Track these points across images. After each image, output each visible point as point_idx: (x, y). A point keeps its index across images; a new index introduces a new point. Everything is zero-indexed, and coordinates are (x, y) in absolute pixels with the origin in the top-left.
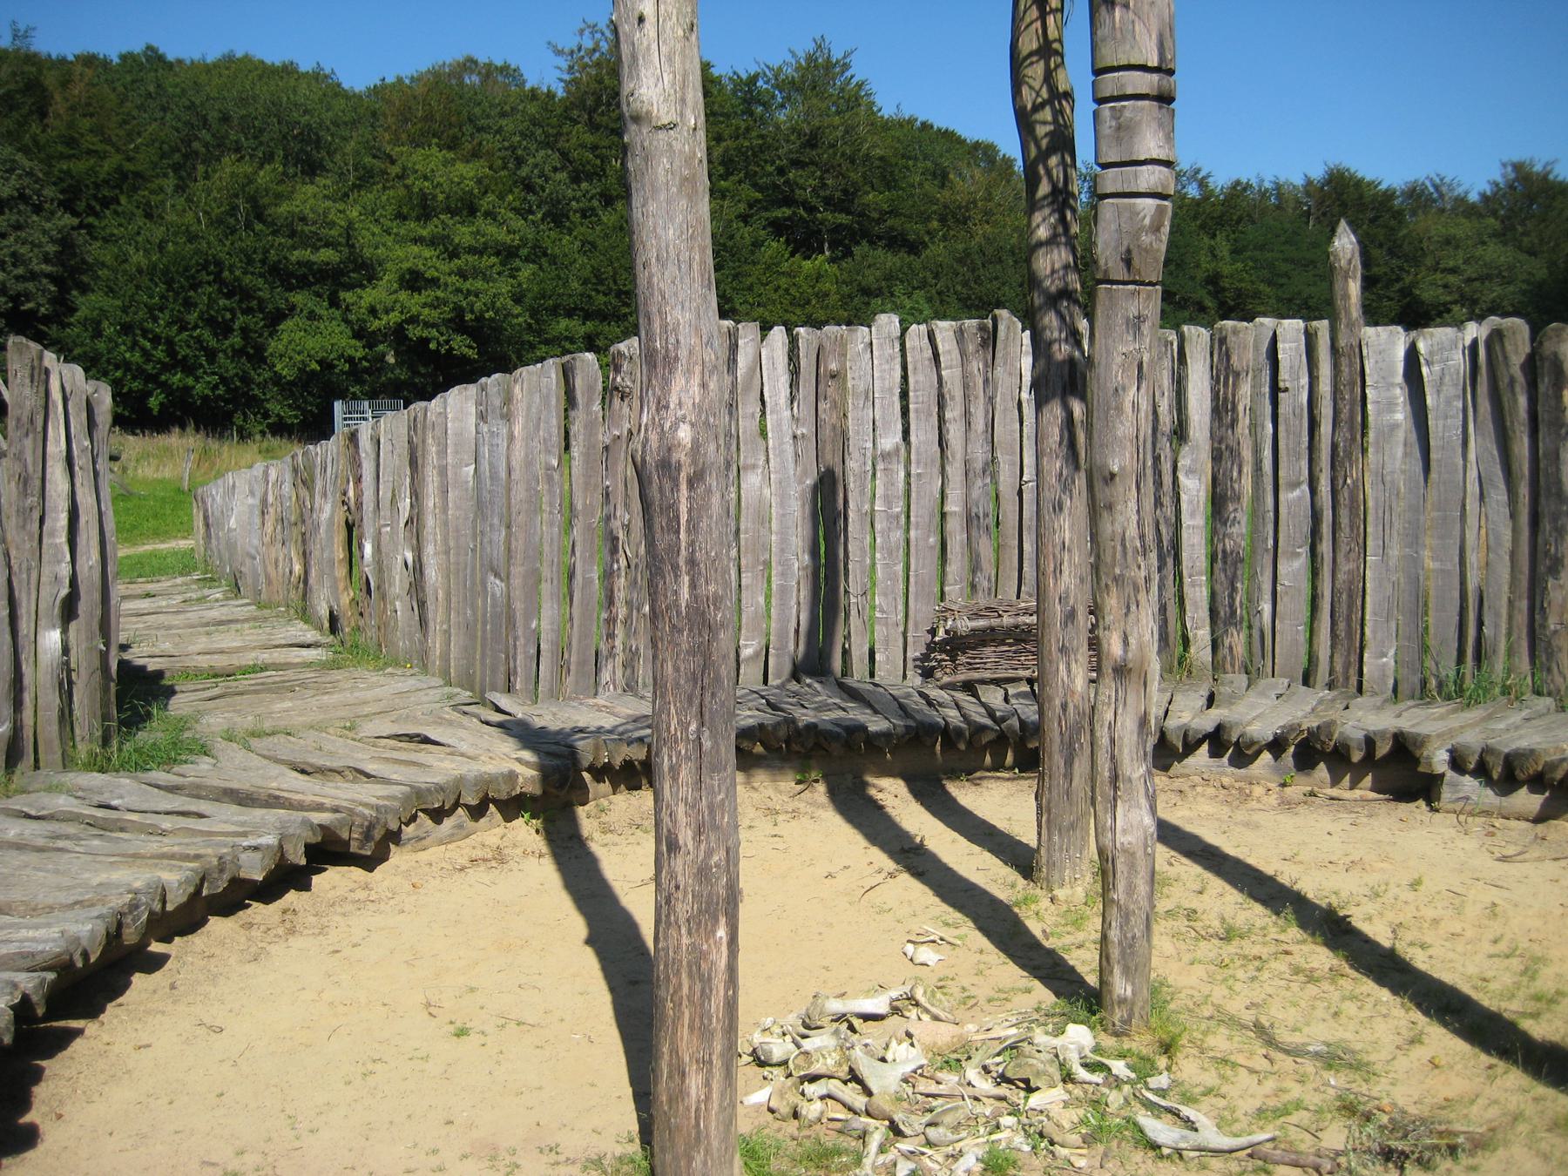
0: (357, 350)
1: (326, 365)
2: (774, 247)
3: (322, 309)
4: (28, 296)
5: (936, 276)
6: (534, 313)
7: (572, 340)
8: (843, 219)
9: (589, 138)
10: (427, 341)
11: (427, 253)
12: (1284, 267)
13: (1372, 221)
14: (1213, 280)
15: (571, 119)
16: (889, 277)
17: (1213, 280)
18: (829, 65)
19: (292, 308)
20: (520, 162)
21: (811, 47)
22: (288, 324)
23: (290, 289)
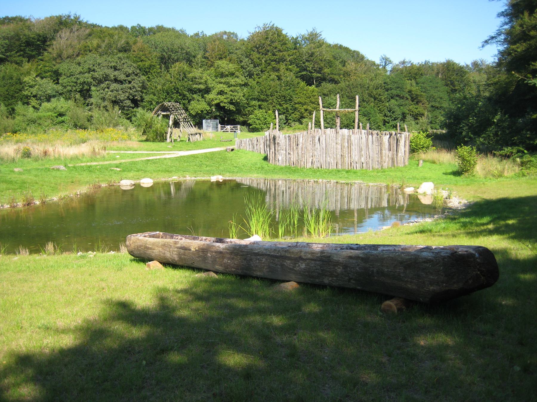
0: (208, 108)
1: (202, 111)
2: (303, 84)
3: (200, 98)
4: (136, 96)
5: (341, 90)
6: (247, 99)
7: (256, 106)
8: (319, 75)
9: (258, 56)
10: (225, 106)
11: (224, 86)
14: (410, 92)
15: (253, 50)
18: (316, 34)
19: (194, 98)
20: (241, 61)
21: (311, 30)
22: (192, 102)
23: (193, 94)
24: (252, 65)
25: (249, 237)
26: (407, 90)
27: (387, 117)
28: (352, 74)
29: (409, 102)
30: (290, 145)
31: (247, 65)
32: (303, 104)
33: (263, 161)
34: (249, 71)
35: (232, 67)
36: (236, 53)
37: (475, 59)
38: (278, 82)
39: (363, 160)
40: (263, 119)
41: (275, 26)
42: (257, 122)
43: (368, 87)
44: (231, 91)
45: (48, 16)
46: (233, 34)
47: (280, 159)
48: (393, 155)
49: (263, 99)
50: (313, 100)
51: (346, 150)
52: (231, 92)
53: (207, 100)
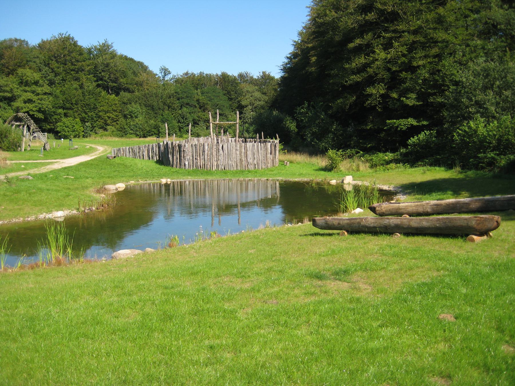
12: (213, 97)
16: (129, 100)
17: (198, 100)
18: (108, 46)
24: (53, 75)
25: (335, 212)
26: (195, 99)
27: (181, 123)
28: (145, 84)
29: (197, 109)
30: (196, 152)
31: (47, 74)
32: (106, 112)
33: (158, 166)
34: (50, 80)
35: (37, 76)
36: (35, 62)
37: (240, 72)
38: (80, 91)
39: (255, 162)
40: (71, 126)
42: (66, 129)
44: (38, 99)
46: (24, 41)
47: (187, 163)
48: (273, 157)
49: (67, 107)
50: (115, 109)
52: (39, 101)
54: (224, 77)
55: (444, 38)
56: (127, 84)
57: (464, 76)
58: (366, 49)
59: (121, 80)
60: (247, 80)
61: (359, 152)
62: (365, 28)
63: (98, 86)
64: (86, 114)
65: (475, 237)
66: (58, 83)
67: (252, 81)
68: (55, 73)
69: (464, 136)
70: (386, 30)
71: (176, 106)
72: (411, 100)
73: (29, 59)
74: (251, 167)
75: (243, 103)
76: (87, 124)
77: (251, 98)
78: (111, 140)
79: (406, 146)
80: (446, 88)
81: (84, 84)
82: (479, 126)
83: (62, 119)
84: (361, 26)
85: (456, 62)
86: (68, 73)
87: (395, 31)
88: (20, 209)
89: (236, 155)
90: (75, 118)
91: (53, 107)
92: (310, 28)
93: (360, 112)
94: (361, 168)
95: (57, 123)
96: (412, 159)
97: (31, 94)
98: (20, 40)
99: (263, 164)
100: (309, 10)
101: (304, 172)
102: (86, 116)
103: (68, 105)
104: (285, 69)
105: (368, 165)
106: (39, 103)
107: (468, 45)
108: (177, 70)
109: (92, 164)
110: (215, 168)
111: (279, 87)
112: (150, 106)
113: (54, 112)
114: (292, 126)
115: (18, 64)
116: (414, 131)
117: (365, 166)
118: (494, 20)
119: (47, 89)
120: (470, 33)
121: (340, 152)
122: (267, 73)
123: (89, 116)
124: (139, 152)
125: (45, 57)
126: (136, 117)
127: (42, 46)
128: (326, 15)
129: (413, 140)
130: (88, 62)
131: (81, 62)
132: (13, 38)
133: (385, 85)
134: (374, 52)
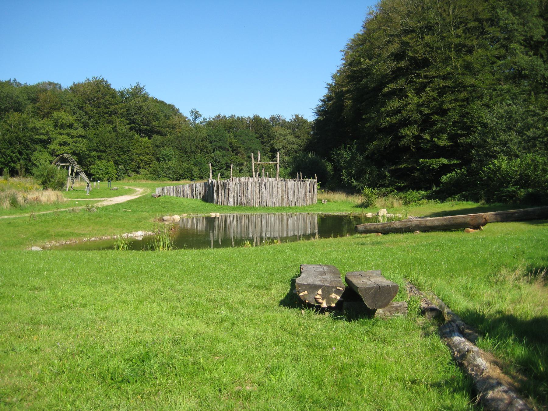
8: (148, 128)
13: (264, 128)
14: (231, 144)
17: (231, 144)
18: (140, 89)
26: (228, 143)
28: (177, 127)
30: (240, 189)
33: (203, 203)
34: (83, 123)
36: (69, 105)
37: (272, 115)
38: (113, 134)
41: (105, 79)
42: (100, 172)
43: (194, 140)
44: (73, 142)
45: (228, 115)
47: (231, 200)
49: (101, 149)
50: (148, 152)
51: (284, 193)
52: (74, 144)
53: (49, 150)
54: (257, 120)
55: (472, 83)
56: (159, 127)
57: (487, 117)
58: (401, 93)
59: (154, 123)
60: (280, 123)
61: (393, 191)
62: (397, 74)
63: (131, 129)
64: (119, 156)
65: (470, 229)
66: (91, 126)
67: (285, 125)
68: (89, 117)
69: (489, 173)
70: (419, 76)
71: (208, 149)
72: (443, 141)
73: (63, 102)
74: (292, 204)
75: (276, 146)
76: (120, 167)
77: (284, 142)
78: (144, 182)
79: (438, 184)
80: (475, 129)
81: (118, 127)
82: (503, 163)
83: (96, 161)
84: (393, 72)
85: (483, 105)
86: (102, 116)
87: (426, 77)
88: (105, 230)
89: (277, 192)
90: (108, 161)
91: (87, 150)
92: (344, 72)
93: (393, 154)
94: (395, 205)
95: (90, 165)
96: (442, 195)
97: (66, 137)
98: (53, 83)
99: (303, 201)
100: (343, 53)
101: (342, 209)
102: (119, 158)
103: (101, 148)
104: (319, 112)
105: (401, 202)
106: (74, 146)
107: (495, 90)
108: (209, 113)
109: (140, 202)
110: (257, 205)
111: (313, 130)
112: (182, 149)
113: (88, 155)
114: (329, 167)
115: (53, 107)
116: (445, 169)
117: (399, 203)
118: (519, 66)
119: (81, 131)
120: (497, 79)
121: (376, 191)
122: (300, 116)
123: (122, 159)
124: (183, 191)
125: (79, 100)
126: (169, 160)
127: (75, 89)
128: (360, 63)
129: (444, 179)
130: (120, 105)
131: (114, 105)
132: (47, 82)
133: (418, 127)
134: (407, 96)
